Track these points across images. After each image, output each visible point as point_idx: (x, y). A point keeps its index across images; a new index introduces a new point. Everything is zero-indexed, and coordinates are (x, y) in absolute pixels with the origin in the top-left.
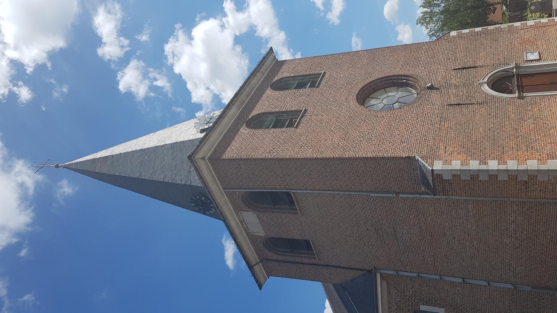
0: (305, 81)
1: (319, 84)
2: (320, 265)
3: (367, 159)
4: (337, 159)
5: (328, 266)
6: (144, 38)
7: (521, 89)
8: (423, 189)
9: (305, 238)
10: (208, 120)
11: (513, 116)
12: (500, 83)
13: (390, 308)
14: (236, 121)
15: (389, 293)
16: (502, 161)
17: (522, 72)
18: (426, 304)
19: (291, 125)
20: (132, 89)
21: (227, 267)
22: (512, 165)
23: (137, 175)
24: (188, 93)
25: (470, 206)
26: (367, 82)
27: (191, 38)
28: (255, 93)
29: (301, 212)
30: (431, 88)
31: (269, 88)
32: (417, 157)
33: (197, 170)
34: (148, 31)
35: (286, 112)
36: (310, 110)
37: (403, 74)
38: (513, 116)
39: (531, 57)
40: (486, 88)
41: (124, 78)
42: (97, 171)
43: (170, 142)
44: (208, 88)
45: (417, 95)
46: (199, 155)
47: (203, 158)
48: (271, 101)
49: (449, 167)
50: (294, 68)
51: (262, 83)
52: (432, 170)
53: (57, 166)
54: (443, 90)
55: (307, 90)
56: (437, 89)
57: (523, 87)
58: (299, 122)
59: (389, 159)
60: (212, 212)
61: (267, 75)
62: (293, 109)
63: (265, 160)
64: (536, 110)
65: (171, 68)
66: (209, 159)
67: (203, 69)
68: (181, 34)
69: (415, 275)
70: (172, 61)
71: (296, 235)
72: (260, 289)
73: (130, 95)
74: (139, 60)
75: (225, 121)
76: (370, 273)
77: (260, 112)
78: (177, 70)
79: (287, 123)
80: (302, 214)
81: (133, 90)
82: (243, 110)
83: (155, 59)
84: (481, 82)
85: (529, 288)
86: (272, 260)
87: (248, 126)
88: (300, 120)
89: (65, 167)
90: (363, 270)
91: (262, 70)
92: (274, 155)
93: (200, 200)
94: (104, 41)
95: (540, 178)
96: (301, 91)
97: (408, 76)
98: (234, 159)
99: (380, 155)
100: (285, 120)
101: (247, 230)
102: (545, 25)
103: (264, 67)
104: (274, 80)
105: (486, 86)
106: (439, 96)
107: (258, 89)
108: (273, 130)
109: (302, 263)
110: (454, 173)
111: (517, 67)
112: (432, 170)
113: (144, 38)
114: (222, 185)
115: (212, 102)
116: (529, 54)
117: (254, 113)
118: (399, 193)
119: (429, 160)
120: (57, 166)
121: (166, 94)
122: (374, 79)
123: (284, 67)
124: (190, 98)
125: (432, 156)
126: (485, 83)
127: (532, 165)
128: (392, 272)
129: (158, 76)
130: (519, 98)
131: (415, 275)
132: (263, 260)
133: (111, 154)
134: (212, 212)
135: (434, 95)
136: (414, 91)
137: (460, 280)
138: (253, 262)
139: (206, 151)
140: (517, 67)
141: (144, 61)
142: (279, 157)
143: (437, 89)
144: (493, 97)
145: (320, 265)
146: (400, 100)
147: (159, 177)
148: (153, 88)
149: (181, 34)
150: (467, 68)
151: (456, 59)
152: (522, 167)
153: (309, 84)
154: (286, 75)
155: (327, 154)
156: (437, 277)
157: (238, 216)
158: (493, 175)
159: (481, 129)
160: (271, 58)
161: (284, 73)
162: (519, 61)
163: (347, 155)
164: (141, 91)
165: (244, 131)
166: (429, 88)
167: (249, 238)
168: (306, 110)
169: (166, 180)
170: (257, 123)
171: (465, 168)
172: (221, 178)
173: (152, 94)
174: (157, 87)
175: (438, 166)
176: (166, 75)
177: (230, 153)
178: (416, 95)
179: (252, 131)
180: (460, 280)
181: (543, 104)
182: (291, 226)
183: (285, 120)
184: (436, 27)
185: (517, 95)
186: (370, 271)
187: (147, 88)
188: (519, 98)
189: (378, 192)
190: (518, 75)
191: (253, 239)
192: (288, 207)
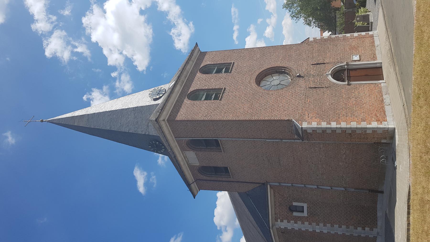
0: (221, 67)
1: (231, 71)
2: (233, 182)
3: (265, 121)
4: (247, 121)
5: (238, 182)
6: (67, 12)
7: (350, 79)
8: (296, 137)
9: (225, 166)
10: (158, 92)
11: (344, 96)
12: (338, 75)
13: (275, 205)
14: (180, 94)
15: (275, 196)
16: (338, 123)
17: (350, 67)
19: (216, 98)
20: (57, 54)
21: (140, 193)
22: (343, 125)
23: (108, 128)
24: (105, 59)
25: (321, 146)
26: (261, 70)
27: (105, 12)
28: (189, 75)
30: (299, 76)
31: (199, 72)
32: (293, 120)
33: (160, 127)
34: (70, 7)
35: (212, 89)
38: (344, 96)
39: (356, 58)
40: (330, 78)
41: (49, 46)
42: (76, 124)
43: (132, 106)
44: (121, 53)
45: (291, 80)
46: (161, 119)
47: (164, 120)
48: (201, 82)
49: (311, 126)
50: (213, 58)
51: (193, 68)
52: (302, 128)
53: (42, 121)
54: (306, 78)
55: (223, 74)
56: (303, 77)
57: (350, 77)
58: (222, 97)
59: (277, 121)
60: (162, 151)
61: (196, 62)
62: (217, 87)
63: (204, 121)
64: (356, 93)
65: (89, 38)
66: (168, 120)
67: (115, 38)
68: (96, 8)
69: (290, 185)
70: (89, 31)
71: (220, 164)
72: (194, 198)
73: (55, 59)
74: (62, 30)
76: (264, 185)
77: (195, 89)
78: (94, 39)
79: (213, 96)
81: (59, 54)
82: (184, 87)
83: (76, 30)
84: (327, 73)
85: (353, 190)
86: (203, 180)
87: (189, 98)
88: (222, 95)
89: (49, 122)
90: (259, 183)
91: (192, 59)
92: (209, 118)
93: (155, 144)
94: (36, 17)
95: (357, 132)
96: (220, 75)
97: (286, 68)
98: (184, 121)
99: (272, 118)
100: (214, 94)
102: (364, 37)
103: (193, 57)
104: (201, 66)
106: (303, 82)
107: (191, 72)
108: (206, 101)
109: (222, 181)
110: (313, 129)
111: (347, 64)
112: (302, 128)
113: (67, 12)
114: (174, 135)
115: (124, 64)
116: (354, 56)
117: (191, 89)
118: (282, 139)
119: (300, 122)
120: (42, 121)
121: (86, 58)
122: (265, 68)
123: (207, 57)
124: (107, 62)
125: (302, 120)
126: (329, 74)
127: (354, 125)
128: (277, 184)
129: (77, 44)
130: (349, 85)
131: (290, 185)
132: (197, 180)
133: (87, 113)
134: (162, 151)
135: (301, 81)
136: (289, 77)
137: (316, 187)
138: (191, 181)
139: (165, 115)
140: (347, 64)
141: (66, 31)
142: (212, 119)
143: (303, 77)
144: (334, 84)
145: (233, 182)
146: (282, 83)
147: (125, 129)
148: (73, 53)
149: (96, 8)
151: (313, 57)
152: (348, 126)
153: (224, 70)
154: (209, 63)
155: (241, 118)
156: (303, 185)
157: (183, 154)
158: (334, 131)
159: (327, 103)
160: (197, 50)
161: (207, 61)
163: (253, 118)
164: (66, 56)
165: (187, 102)
166: (298, 76)
167: (189, 167)
168: (225, 88)
169: (131, 131)
170: (195, 96)
171: (319, 126)
172: (174, 131)
173: (75, 58)
174: (77, 53)
175: (305, 125)
176: (85, 43)
177: (181, 116)
178: (290, 80)
179: (193, 102)
180: (316, 187)
181: (360, 89)
182: (216, 159)
183: (214, 94)
184: (296, 11)
185: (347, 83)
186: (264, 184)
187: (70, 53)
188: (349, 85)
189: (271, 139)
191: (191, 168)
192: (215, 148)
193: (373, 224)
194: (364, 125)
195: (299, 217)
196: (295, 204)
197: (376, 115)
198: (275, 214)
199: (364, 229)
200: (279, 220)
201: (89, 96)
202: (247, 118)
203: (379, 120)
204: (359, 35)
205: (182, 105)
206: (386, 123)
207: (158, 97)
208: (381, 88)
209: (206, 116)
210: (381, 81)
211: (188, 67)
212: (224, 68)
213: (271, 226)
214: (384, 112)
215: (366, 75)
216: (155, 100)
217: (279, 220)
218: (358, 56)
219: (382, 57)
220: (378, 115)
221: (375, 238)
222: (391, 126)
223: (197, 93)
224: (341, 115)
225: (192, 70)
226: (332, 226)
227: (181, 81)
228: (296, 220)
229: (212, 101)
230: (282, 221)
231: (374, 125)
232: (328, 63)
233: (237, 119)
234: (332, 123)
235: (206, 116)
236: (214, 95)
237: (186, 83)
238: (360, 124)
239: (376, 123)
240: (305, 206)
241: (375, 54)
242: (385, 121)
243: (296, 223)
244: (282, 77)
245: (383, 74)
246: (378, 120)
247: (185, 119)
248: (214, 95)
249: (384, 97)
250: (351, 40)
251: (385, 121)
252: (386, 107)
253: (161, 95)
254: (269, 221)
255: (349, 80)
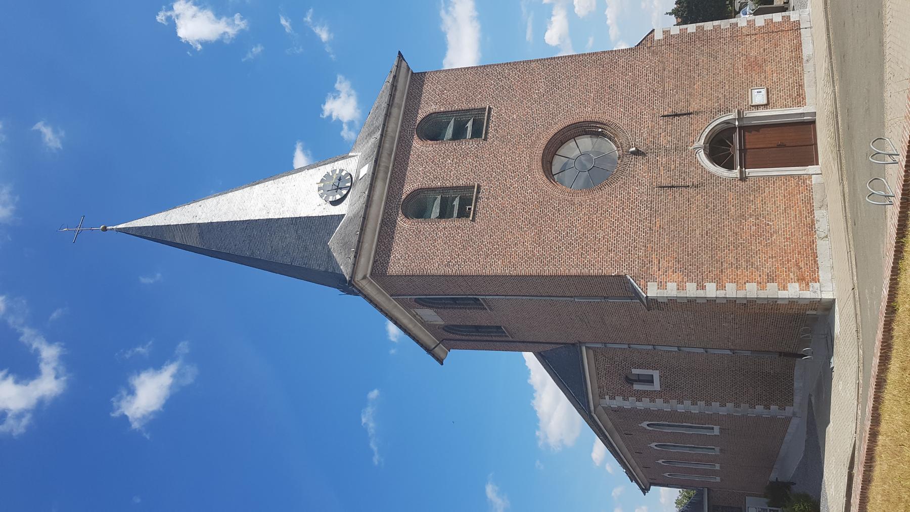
1: (486, 133)
14: (386, 203)
15: (596, 360)
17: (746, 123)
18: (639, 367)
28: (397, 146)
29: (489, 306)
30: (637, 153)
31: (415, 136)
32: (629, 277)
35: (452, 188)
36: (485, 186)
37: (597, 119)
39: (759, 97)
40: (702, 157)
46: (359, 276)
47: (365, 277)
51: (402, 126)
53: (105, 229)
55: (469, 145)
56: (643, 154)
57: (745, 149)
66: (371, 274)
75: (374, 210)
80: (491, 309)
82: (390, 182)
85: (749, 353)
95: (758, 302)
100: (458, 203)
101: (423, 323)
103: (398, 94)
104: (419, 119)
105: (702, 153)
107: (400, 137)
120: (105, 229)
127: (752, 291)
128: (599, 346)
131: (626, 346)
135: (640, 165)
140: (740, 118)
143: (643, 154)
150: (679, 115)
154: (433, 108)
155: (523, 270)
159: (698, 232)
162: (742, 106)
166: (633, 153)
168: (479, 187)
169: (296, 264)
170: (417, 207)
175: (653, 291)
177: (397, 265)
180: (676, 349)
183: (458, 203)
188: (743, 178)
190: (740, 128)
191: (430, 327)
193: (786, 397)
194: (772, 291)
195: (644, 392)
196: (635, 371)
197: (797, 265)
198: (599, 387)
199: (767, 407)
200: (607, 397)
201: (169, 14)
202: (534, 269)
203: (803, 279)
204: (769, 23)
205: (394, 233)
206: (817, 285)
207: (338, 197)
208: (809, 189)
209: (448, 265)
210: (811, 169)
211: (391, 126)
212: (469, 125)
213: (592, 408)
214: (815, 256)
215: (779, 146)
216: (335, 203)
217: (607, 397)
218: (764, 91)
219: (817, 101)
220: (802, 265)
221: (788, 420)
222: (827, 295)
223: (422, 195)
224: (725, 265)
225: (400, 132)
226: (708, 404)
227: (382, 169)
228: (639, 396)
229: (458, 223)
230: (612, 398)
231: (793, 291)
232: (697, 113)
233: (514, 273)
234: (707, 284)
235: (448, 265)
236: (457, 200)
237: (393, 170)
238: (763, 288)
239: (797, 285)
240: (656, 375)
241: (801, 86)
242: (816, 280)
243: (639, 400)
244: (598, 141)
245: (816, 144)
246: (801, 279)
247: (408, 273)
248: (457, 200)
249: (818, 214)
250: (748, 38)
251: (816, 280)
252: (819, 243)
253: (344, 192)
254: (588, 402)
255: (744, 165)
